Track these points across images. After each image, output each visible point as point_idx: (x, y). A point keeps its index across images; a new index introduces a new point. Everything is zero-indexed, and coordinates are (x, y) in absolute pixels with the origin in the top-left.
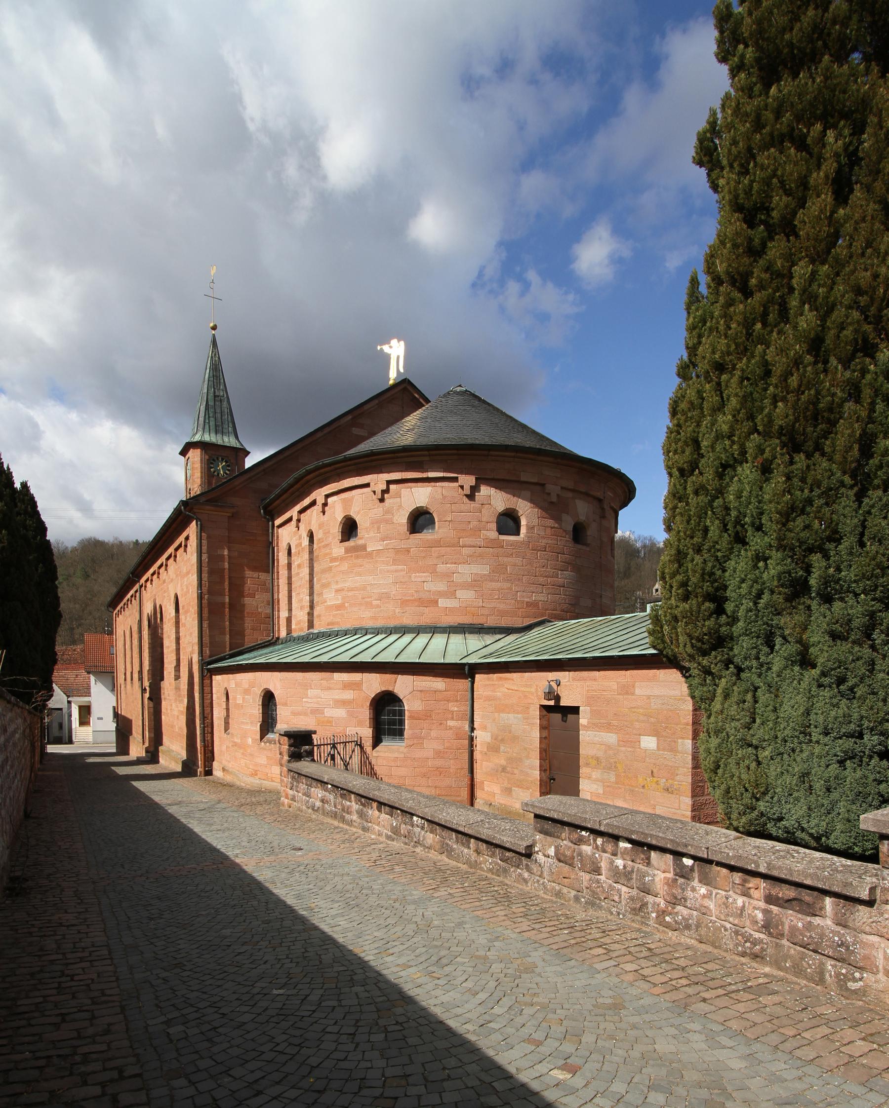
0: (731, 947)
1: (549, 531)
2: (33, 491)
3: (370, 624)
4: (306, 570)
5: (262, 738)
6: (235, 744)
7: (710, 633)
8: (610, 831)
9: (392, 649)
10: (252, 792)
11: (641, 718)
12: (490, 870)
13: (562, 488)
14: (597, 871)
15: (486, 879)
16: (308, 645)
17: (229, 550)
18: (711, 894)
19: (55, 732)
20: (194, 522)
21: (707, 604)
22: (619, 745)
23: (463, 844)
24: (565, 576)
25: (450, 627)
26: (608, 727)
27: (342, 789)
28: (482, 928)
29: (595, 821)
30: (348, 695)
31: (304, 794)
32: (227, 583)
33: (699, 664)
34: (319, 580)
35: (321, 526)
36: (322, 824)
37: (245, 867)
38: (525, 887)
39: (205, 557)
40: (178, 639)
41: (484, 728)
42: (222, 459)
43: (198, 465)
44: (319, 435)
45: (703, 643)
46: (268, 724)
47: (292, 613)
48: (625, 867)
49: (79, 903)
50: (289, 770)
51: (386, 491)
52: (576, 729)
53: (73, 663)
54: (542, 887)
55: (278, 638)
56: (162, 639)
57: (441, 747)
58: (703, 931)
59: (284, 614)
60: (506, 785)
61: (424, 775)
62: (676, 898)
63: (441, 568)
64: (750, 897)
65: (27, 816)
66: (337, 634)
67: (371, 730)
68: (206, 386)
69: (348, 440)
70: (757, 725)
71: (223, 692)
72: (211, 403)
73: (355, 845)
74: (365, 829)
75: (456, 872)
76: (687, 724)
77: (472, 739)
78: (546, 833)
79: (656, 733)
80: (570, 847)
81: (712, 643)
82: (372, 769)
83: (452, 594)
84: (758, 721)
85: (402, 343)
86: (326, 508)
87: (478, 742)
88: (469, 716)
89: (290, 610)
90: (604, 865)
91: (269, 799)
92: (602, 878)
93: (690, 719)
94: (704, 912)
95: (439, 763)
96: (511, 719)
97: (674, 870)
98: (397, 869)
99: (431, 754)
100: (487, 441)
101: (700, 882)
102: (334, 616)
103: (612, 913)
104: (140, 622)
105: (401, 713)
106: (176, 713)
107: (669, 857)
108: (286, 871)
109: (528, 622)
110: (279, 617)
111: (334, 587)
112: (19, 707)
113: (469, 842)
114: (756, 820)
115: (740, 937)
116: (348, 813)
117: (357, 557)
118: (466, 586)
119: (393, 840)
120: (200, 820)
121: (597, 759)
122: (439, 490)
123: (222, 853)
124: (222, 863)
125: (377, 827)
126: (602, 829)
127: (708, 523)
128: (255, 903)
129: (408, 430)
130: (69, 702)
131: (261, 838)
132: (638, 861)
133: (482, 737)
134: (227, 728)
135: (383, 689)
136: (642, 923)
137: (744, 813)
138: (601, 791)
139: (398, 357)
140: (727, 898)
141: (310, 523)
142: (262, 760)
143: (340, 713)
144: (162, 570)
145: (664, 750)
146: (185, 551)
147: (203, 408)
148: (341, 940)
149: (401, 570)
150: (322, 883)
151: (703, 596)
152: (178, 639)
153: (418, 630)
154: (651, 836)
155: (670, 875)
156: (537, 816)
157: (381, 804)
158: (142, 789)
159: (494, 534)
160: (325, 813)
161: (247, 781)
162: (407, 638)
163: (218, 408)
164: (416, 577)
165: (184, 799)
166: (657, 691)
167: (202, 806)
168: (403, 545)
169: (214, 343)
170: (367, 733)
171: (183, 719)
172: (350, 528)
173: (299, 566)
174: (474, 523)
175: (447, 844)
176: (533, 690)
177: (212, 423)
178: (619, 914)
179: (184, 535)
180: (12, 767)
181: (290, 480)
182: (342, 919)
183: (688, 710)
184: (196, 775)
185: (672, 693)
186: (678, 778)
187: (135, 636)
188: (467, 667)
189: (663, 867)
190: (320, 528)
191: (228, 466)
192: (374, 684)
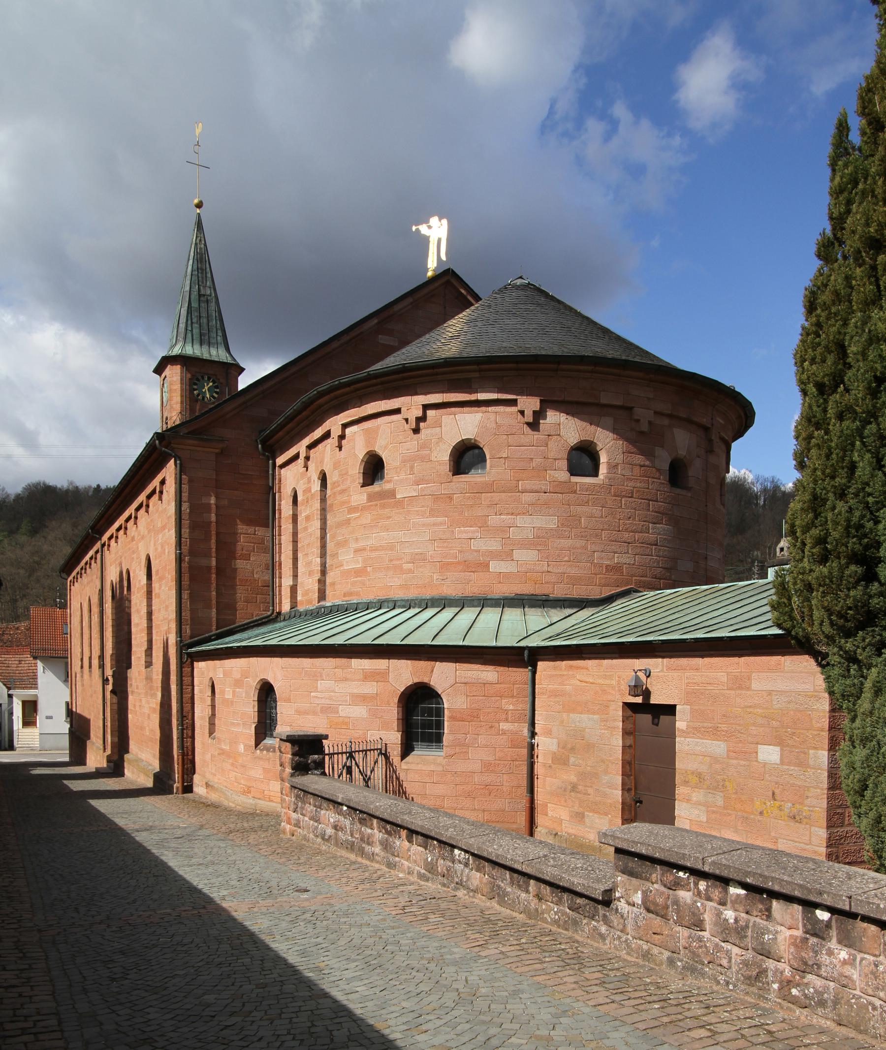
1: (637, 470)
3: (399, 595)
5: (257, 745)
6: (223, 752)
7: (856, 606)
8: (717, 872)
9: (427, 627)
11: (760, 720)
13: (656, 413)
14: (699, 925)
16: (319, 622)
17: (217, 498)
18: (854, 960)
20: (172, 461)
21: (853, 568)
22: (728, 757)
23: (519, 887)
24: (658, 531)
25: (505, 599)
26: (714, 733)
27: (361, 812)
28: (546, 999)
29: (696, 858)
30: (370, 688)
31: (311, 818)
32: (213, 541)
33: (841, 648)
35: (336, 465)
36: (335, 857)
37: (234, 914)
38: (601, 945)
39: (185, 506)
40: (150, 614)
41: (548, 733)
42: (209, 379)
43: (177, 387)
45: (847, 620)
46: (265, 725)
47: (298, 580)
48: (736, 920)
51: (422, 419)
52: (671, 734)
54: (624, 945)
55: (279, 613)
56: (129, 615)
58: (843, 1009)
60: (576, 808)
61: (469, 795)
62: (806, 964)
66: (356, 608)
68: (188, 282)
71: (207, 683)
72: (195, 305)
73: (378, 886)
74: (391, 865)
75: (510, 923)
77: (532, 747)
78: (631, 873)
79: (779, 742)
80: (662, 893)
82: (401, 785)
83: (507, 556)
85: (445, 222)
86: (344, 442)
87: (540, 751)
89: (295, 576)
91: (266, 825)
92: (706, 934)
93: (825, 723)
94: (845, 983)
95: (488, 778)
96: (585, 721)
97: (804, 926)
98: (433, 918)
99: (477, 767)
100: (556, 350)
101: (840, 942)
103: (718, 983)
104: (101, 591)
105: (440, 712)
106: (146, 711)
107: (798, 909)
108: (288, 918)
109: (607, 592)
110: (280, 586)
113: (528, 885)
116: (369, 844)
117: (383, 506)
118: (525, 544)
119: (427, 880)
120: (176, 851)
121: (700, 775)
122: (492, 417)
123: (204, 894)
124: (204, 907)
125: (406, 863)
126: (706, 869)
127: (856, 457)
128: (247, 961)
129: (451, 338)
130: (10, 696)
131: (256, 876)
132: (755, 913)
133: (545, 744)
134: (211, 732)
135: (416, 680)
136: (760, 996)
139: (439, 241)
140: (876, 966)
141: (322, 462)
142: (257, 772)
143: (359, 712)
144: (130, 524)
145: (789, 764)
146: (160, 499)
149: (441, 524)
152: (150, 614)
153: (462, 603)
154: (773, 879)
155: (799, 933)
156: (618, 851)
157: (412, 832)
158: (102, 810)
159: (563, 475)
160: (339, 844)
161: (237, 800)
162: (448, 613)
163: (204, 312)
164: (460, 532)
165: (157, 823)
167: (179, 833)
168: (445, 490)
169: (199, 225)
170: (394, 738)
172: (374, 468)
173: (308, 518)
174: (537, 461)
175: (499, 887)
176: (614, 682)
177: (196, 331)
178: (728, 983)
179: (159, 477)
181: (296, 405)
182: (359, 983)
183: (824, 711)
184: (171, 793)
186: (808, 802)
187: (95, 610)
188: (526, 653)
190: (335, 468)
191: (217, 387)
192: (404, 674)
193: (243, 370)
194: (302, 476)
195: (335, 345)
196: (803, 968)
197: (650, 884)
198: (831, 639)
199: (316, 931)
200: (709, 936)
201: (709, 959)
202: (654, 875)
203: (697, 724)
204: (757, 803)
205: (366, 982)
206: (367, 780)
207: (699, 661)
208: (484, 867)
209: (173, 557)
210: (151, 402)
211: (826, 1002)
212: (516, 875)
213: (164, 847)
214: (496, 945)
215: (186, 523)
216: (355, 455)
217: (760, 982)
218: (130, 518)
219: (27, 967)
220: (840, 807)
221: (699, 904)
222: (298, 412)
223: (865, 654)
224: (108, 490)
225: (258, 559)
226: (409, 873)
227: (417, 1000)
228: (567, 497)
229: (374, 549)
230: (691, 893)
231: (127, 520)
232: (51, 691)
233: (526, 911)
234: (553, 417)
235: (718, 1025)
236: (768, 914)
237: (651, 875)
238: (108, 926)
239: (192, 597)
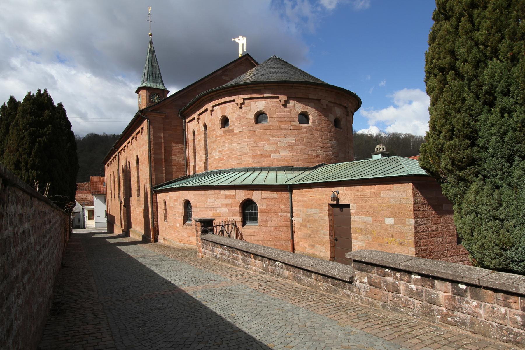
0: (498, 336)
1: (323, 122)
2: (65, 107)
5: (184, 224)
6: (170, 227)
7: (468, 157)
8: (407, 269)
9: (250, 179)
10: (183, 250)
11: (385, 208)
12: (326, 290)
13: (329, 102)
14: (398, 291)
15: (324, 295)
16: (206, 178)
17: (164, 134)
18: (481, 305)
19: (76, 223)
20: (146, 120)
21: (466, 141)
22: (373, 222)
23: (307, 276)
24: (331, 143)
25: (277, 168)
26: (367, 214)
27: (232, 248)
28: (337, 326)
29: (396, 264)
30: (229, 201)
31: (210, 251)
32: (163, 149)
33: (456, 175)
34: (210, 147)
35: (210, 121)
36: (222, 266)
37: (187, 292)
38: (348, 300)
39: (152, 137)
41: (298, 216)
43: (145, 97)
44: (206, 79)
45: (462, 163)
46: (187, 216)
47: (196, 162)
48: (417, 289)
49: (95, 318)
50: (202, 239)
51: (243, 103)
53: (84, 191)
54: (360, 299)
55: (189, 175)
56: (130, 177)
58: (476, 327)
60: (311, 243)
61: (268, 240)
62: (455, 307)
63: (272, 140)
64: (510, 307)
65: (63, 266)
66: (220, 172)
67: (240, 218)
68: (147, 61)
69: (223, 80)
70: (503, 208)
72: (150, 69)
73: (244, 277)
74: (246, 268)
75: (306, 292)
77: (292, 221)
78: (362, 270)
79: (393, 216)
80: (378, 278)
81: (468, 163)
82: (242, 237)
83: (278, 152)
84: (504, 205)
85: (245, 38)
86: (213, 112)
88: (290, 210)
89: (195, 162)
90: (402, 288)
91: (190, 254)
92: (401, 295)
93: (412, 208)
94: (475, 315)
95: (276, 233)
96: (313, 211)
97: (453, 291)
98: (273, 290)
99: (271, 229)
100: (292, 79)
101: (472, 298)
102: (218, 164)
103: (409, 315)
104: (118, 170)
105: (256, 209)
106: (138, 212)
107: (449, 284)
108: (211, 293)
109: (315, 165)
111: (218, 150)
112: (58, 210)
113: (312, 275)
114: (503, 262)
115: (504, 331)
117: (229, 135)
118: (284, 148)
119: (264, 274)
120: (156, 265)
121: (361, 229)
122: (269, 103)
123: (173, 284)
124: (174, 290)
126: (401, 268)
127: (465, 95)
128: (199, 314)
129: (249, 76)
130: (83, 209)
131: (192, 275)
132: (426, 286)
133: (297, 220)
135: (246, 198)
136: (430, 321)
137: (495, 258)
138: (364, 245)
139: (243, 44)
140: (493, 308)
141: (204, 120)
142: (185, 234)
143: (225, 210)
145: (398, 224)
146: (141, 135)
147: (146, 71)
148: (258, 338)
150: (233, 301)
151: (463, 137)
153: (261, 170)
154: (436, 272)
155: (450, 294)
157: (256, 255)
158: (123, 250)
159: (297, 123)
161: (177, 244)
162: (256, 174)
163: (154, 72)
165: (146, 255)
166: (393, 195)
167: (156, 258)
168: (252, 129)
169: (151, 42)
170: (238, 219)
172: (225, 121)
173: (199, 141)
175: (297, 276)
176: (324, 196)
177: (151, 78)
178: (413, 315)
179: (141, 127)
180: (54, 242)
181: (194, 99)
182: (253, 323)
185: (401, 196)
187: (116, 176)
188: (288, 187)
189: (444, 289)
190: (210, 122)
192: (242, 195)
193: (169, 92)
194: (196, 125)
196: (453, 309)
198: (450, 172)
199: (225, 299)
201: (403, 305)
202: (373, 271)
203: (359, 211)
204: (386, 239)
205: (255, 322)
206: (229, 235)
209: (147, 155)
210: (133, 102)
211: (466, 323)
212: (305, 272)
213: (151, 264)
214: (304, 302)
215: (152, 143)
216: (217, 117)
218: (129, 142)
219: (98, 322)
220: (419, 239)
222: (195, 102)
223: (470, 177)
224: (118, 136)
227: (281, 330)
228: (298, 131)
229: (226, 151)
233: (311, 286)
234: (292, 103)
235: (421, 336)
238: (133, 300)
239: (155, 170)
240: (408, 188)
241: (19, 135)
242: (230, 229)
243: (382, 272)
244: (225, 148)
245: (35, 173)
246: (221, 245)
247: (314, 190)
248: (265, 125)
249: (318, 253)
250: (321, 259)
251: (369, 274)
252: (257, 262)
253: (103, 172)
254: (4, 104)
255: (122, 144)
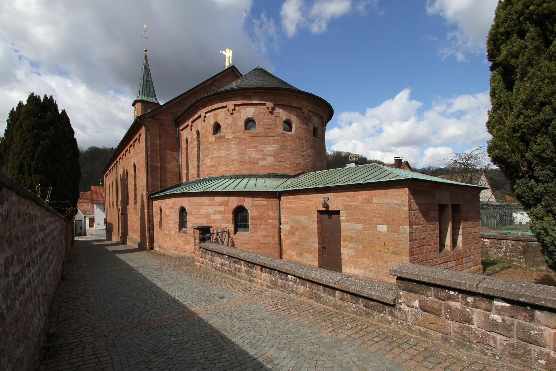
2: (68, 114)
3: (228, 174)
4: (195, 150)
5: (179, 231)
6: (166, 234)
10: (178, 258)
14: (470, 321)
16: (199, 185)
19: (79, 231)
23: (329, 294)
25: (264, 175)
26: (358, 221)
27: (235, 258)
30: (222, 208)
35: (203, 127)
40: (135, 185)
41: (286, 223)
46: (183, 223)
47: (189, 170)
48: (503, 320)
51: (234, 110)
52: (339, 222)
53: (86, 200)
55: (182, 183)
56: (127, 185)
57: (266, 233)
59: (184, 171)
60: (299, 251)
63: (259, 146)
65: (63, 278)
71: (158, 208)
72: (145, 83)
74: (250, 281)
76: (406, 218)
77: (280, 229)
78: (411, 291)
79: (386, 223)
80: (437, 302)
83: (264, 159)
85: (231, 51)
87: (283, 230)
89: (188, 169)
92: (474, 327)
103: (486, 354)
105: (247, 216)
106: (135, 220)
112: (57, 216)
116: (239, 272)
117: (221, 142)
118: (270, 155)
119: (272, 288)
121: (351, 237)
122: (258, 109)
123: (181, 303)
125: (259, 281)
126: (481, 291)
130: (85, 217)
132: (519, 317)
135: (239, 205)
141: (197, 127)
142: (180, 242)
143: (218, 217)
144: (127, 153)
145: (392, 232)
149: (242, 148)
152: (135, 185)
153: (250, 177)
154: (545, 300)
156: (399, 278)
157: (262, 267)
159: (281, 131)
160: (222, 271)
163: (147, 86)
166: (386, 201)
170: (231, 227)
171: (138, 223)
172: (217, 128)
173: (192, 148)
174: (273, 125)
175: (316, 293)
177: (146, 92)
178: (494, 355)
181: (189, 105)
183: (406, 210)
184: (145, 250)
185: (396, 201)
186: (401, 246)
187: (115, 185)
192: (234, 202)
195: (198, 88)
197: (425, 297)
200: (476, 328)
201: (478, 340)
202: (429, 293)
207: (350, 193)
208: (306, 284)
212: (327, 288)
217: (524, 357)
221: (468, 310)
225: (174, 163)
226: (262, 285)
230: (460, 303)
231: (126, 152)
232: (99, 215)
233: (335, 306)
234: (278, 110)
236: (532, 318)
237: (426, 292)
239: (152, 177)
240: (404, 193)
241: (23, 137)
242: (224, 237)
243: (445, 294)
244: (216, 155)
245: (38, 177)
246: (222, 254)
247: (303, 196)
248: (254, 132)
249: (306, 262)
250: (310, 267)
251: (422, 296)
252: (264, 274)
253: (103, 182)
254: (13, 109)
255: (120, 153)
